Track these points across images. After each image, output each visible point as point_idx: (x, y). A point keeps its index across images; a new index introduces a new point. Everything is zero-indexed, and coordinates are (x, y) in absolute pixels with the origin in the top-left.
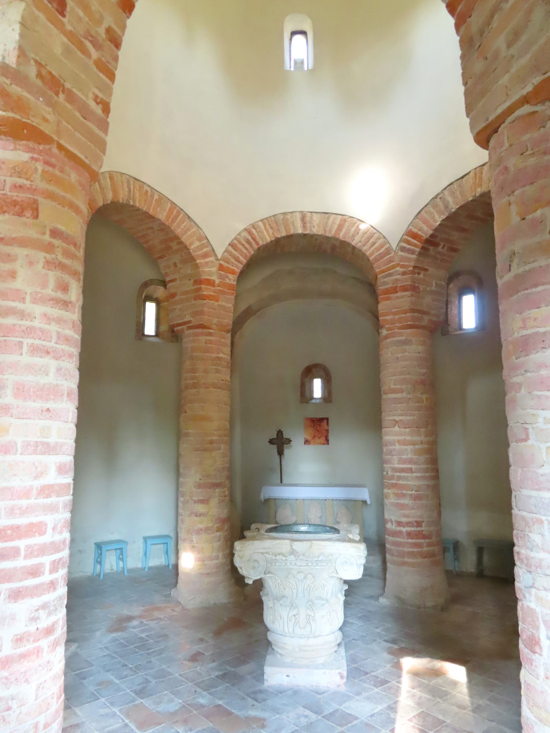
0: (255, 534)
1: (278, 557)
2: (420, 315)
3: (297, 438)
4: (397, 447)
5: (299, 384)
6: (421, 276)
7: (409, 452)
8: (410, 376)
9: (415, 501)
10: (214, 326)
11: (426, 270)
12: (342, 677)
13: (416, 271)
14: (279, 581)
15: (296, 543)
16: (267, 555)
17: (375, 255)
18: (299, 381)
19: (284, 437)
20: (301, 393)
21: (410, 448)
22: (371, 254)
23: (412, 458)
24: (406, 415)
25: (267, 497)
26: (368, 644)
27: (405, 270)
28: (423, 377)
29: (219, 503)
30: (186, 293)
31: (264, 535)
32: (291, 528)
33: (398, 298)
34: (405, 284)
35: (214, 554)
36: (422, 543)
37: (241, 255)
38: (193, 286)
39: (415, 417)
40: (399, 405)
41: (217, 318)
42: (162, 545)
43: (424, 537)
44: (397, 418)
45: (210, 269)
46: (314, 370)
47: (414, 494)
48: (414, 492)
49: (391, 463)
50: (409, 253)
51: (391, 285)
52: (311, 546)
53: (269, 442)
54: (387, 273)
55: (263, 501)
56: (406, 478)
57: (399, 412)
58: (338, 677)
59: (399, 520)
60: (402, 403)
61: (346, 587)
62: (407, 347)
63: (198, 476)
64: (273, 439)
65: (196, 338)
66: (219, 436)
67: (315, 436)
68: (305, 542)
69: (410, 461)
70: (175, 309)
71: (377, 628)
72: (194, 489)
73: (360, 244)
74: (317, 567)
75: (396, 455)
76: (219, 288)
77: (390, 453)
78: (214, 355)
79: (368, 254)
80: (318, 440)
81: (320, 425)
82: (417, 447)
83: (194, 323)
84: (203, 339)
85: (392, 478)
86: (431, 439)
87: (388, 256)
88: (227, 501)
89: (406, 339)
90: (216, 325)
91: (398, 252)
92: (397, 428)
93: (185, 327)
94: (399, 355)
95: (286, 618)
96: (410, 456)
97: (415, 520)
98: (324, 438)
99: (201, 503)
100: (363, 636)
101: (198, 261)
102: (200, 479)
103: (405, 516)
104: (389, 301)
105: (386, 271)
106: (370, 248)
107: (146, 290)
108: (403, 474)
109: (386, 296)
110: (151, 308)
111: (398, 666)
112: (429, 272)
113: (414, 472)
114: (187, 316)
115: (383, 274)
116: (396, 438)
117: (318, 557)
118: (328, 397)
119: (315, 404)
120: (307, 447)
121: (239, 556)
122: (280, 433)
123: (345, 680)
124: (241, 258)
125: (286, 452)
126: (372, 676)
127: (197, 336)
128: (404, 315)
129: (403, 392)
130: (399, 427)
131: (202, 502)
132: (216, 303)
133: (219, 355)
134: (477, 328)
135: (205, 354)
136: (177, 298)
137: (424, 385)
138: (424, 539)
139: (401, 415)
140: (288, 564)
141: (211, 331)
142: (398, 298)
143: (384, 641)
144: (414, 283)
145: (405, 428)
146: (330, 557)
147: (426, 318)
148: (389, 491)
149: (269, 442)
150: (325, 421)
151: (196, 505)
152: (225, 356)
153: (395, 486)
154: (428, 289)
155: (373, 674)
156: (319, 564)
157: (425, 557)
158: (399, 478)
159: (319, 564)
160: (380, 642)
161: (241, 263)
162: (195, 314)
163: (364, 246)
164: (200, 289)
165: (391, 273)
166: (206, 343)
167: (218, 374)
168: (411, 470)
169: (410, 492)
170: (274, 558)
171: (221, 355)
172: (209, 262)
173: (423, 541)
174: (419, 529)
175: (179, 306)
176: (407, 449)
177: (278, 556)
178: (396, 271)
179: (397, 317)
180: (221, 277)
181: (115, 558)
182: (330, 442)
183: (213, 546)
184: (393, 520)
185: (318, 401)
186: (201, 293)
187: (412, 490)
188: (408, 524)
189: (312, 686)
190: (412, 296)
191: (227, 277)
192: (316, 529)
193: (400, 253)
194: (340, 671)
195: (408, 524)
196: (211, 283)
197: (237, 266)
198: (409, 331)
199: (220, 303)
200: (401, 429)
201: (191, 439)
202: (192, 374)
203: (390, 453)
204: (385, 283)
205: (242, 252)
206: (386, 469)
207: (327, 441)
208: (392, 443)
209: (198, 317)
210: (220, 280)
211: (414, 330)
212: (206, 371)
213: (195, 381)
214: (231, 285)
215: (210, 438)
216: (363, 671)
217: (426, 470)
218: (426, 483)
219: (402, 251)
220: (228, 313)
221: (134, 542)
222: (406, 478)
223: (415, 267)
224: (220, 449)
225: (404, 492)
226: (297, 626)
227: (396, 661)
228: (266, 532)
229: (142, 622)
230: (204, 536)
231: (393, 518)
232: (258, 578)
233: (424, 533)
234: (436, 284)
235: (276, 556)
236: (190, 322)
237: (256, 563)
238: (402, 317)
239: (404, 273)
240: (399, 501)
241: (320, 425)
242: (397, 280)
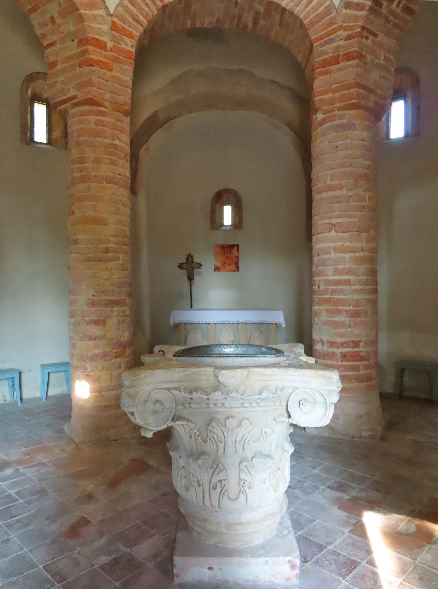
0: (158, 359)
1: (195, 395)
2: (366, 93)
3: (208, 261)
4: (333, 255)
5: (209, 210)
6: (369, 42)
7: (347, 260)
8: (351, 169)
9: (352, 317)
10: (107, 104)
11: (376, 35)
12: (293, 567)
13: (365, 34)
14: (196, 430)
15: (224, 372)
16: (176, 392)
17: (311, 17)
19: (195, 261)
20: (211, 219)
21: (348, 255)
22: (306, 17)
23: (350, 268)
24: (345, 216)
25: (177, 321)
26: (309, 494)
27: (349, 32)
28: (366, 171)
29: (119, 324)
30: (69, 59)
31: (172, 360)
32: (211, 350)
33: (340, 69)
34: (350, 50)
35: (113, 383)
36: (359, 366)
37: (141, 13)
38: (77, 49)
39: (356, 220)
40: (337, 205)
41: (112, 92)
42: (63, 374)
43: (361, 359)
44: (334, 221)
45: (100, 26)
46: (224, 195)
47: (352, 310)
48: (351, 308)
49: (325, 276)
50: (356, 10)
51: (331, 55)
52: (247, 376)
53: (179, 266)
54: (326, 39)
55: (173, 325)
56: (342, 292)
57: (337, 213)
58: (287, 568)
59: (333, 340)
60: (340, 202)
61: (291, 430)
62: (349, 133)
63: (91, 292)
64: (183, 263)
65: (83, 117)
66: (116, 244)
67: (225, 263)
68: (239, 370)
69: (349, 272)
70: (56, 82)
71: (314, 468)
72: (86, 308)
73: (292, 4)
74: (257, 409)
75: (331, 266)
76: (112, 54)
77: (324, 263)
78: (108, 141)
79: (301, 16)
80: (228, 267)
81: (230, 252)
82: (357, 254)
83: (81, 96)
84: (93, 118)
85: (326, 292)
86: (371, 245)
87: (328, 17)
88: (128, 321)
89: (348, 124)
90: (110, 102)
91: (341, 11)
92: (333, 233)
93: (68, 104)
94: (339, 143)
95: (207, 485)
96: (348, 266)
97: (351, 339)
98: (234, 265)
99: (95, 324)
100: (300, 480)
101: (82, 11)
102: (94, 296)
103: (341, 336)
104: (328, 75)
105: (325, 37)
106: (305, 8)
107: (31, 86)
108: (339, 287)
109: (324, 69)
110: (40, 111)
111: (359, 530)
112: (379, 39)
113: (352, 285)
114: (71, 90)
115: (321, 41)
116: (332, 245)
117: (260, 393)
119: (225, 230)
120: (217, 273)
121: (130, 396)
122: (190, 257)
123: (297, 571)
124: (141, 17)
126: (328, 552)
127: (85, 115)
128: (347, 92)
129: (342, 189)
130: (336, 232)
131: (96, 322)
132: (109, 74)
133: (114, 142)
134: (407, 135)
135: (95, 139)
136: (59, 67)
137: (368, 180)
138: (361, 361)
139: (339, 217)
140: (211, 406)
141: (103, 109)
142: (340, 69)
143: (328, 487)
144: (362, 50)
145: (344, 232)
146: (279, 393)
147: (373, 98)
148: (321, 308)
150: (236, 248)
151: (89, 327)
152: (124, 145)
153: (327, 301)
154: (376, 61)
155: (329, 547)
156: (262, 404)
157: (361, 382)
158: (334, 292)
159: (262, 404)
160: (324, 490)
161: (142, 26)
162: (81, 86)
163: (297, 6)
164: (86, 51)
165: (331, 39)
166: (96, 125)
167: (112, 166)
168: (348, 282)
169: (347, 308)
170: (188, 396)
171: (117, 142)
172: (97, 15)
173: (360, 363)
174: (356, 350)
175: (62, 78)
176: (345, 258)
177: (194, 394)
178: (339, 36)
179: (338, 95)
180: (114, 39)
181: (7, 388)
182: (241, 265)
183: (112, 374)
184: (325, 341)
185: (228, 228)
186: (87, 56)
187: (350, 306)
188: (343, 344)
189: (248, 581)
190: (358, 66)
191: (123, 40)
192: (247, 350)
193: (344, 11)
194: (291, 558)
195: (343, 344)
196: (101, 45)
197: (135, 29)
198: (352, 112)
199: (114, 73)
200: (339, 234)
201: (81, 246)
202: (80, 165)
203: (324, 263)
204: (322, 53)
205: (141, 9)
206: (317, 283)
208: (327, 251)
209: (84, 90)
210: (114, 43)
211: (360, 111)
212: (97, 161)
213: (83, 174)
214: (128, 51)
215: (104, 246)
216: (315, 543)
217: (366, 283)
218: (366, 297)
219: (346, 8)
220: (125, 89)
221: (30, 370)
222: (342, 292)
223: (363, 28)
224: (118, 259)
225: (340, 308)
226: (225, 497)
227: (354, 521)
228: (174, 356)
229: (17, 470)
230: (101, 363)
231: (325, 338)
232: (164, 427)
233: (361, 354)
234: (385, 56)
235: (191, 392)
236: (75, 97)
237: (158, 405)
238: (344, 94)
239: (349, 37)
240: (333, 319)
241: (230, 252)
242: (339, 47)
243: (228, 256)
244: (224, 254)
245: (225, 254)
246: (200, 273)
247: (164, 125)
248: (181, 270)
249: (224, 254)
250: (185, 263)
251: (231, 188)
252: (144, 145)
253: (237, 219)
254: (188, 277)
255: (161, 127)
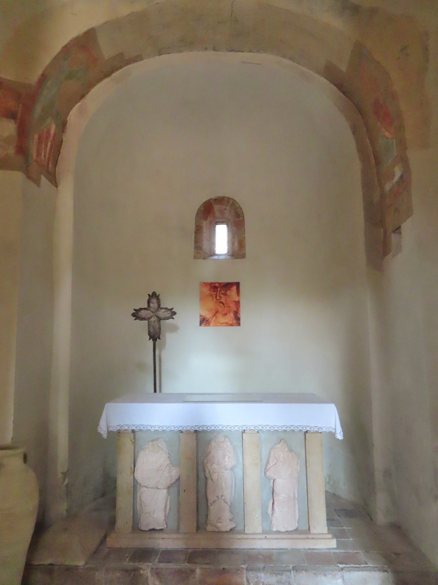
18: (192, 226)
25: (115, 425)
46: (216, 208)
53: (133, 315)
64: (141, 309)
67: (217, 312)
80: (222, 320)
81: (225, 294)
98: (232, 315)
118: (238, 251)
120: (204, 328)
125: (169, 338)
149: (133, 315)
150: (234, 288)
207: (237, 321)
241: (225, 294)
243: (222, 300)
244: (216, 297)
245: (218, 298)
246: (175, 329)
247: (113, 71)
248: (137, 321)
249: (216, 297)
250: (144, 309)
251: (227, 196)
252: (76, 103)
253: (236, 244)
254: (149, 334)
255: (108, 75)
